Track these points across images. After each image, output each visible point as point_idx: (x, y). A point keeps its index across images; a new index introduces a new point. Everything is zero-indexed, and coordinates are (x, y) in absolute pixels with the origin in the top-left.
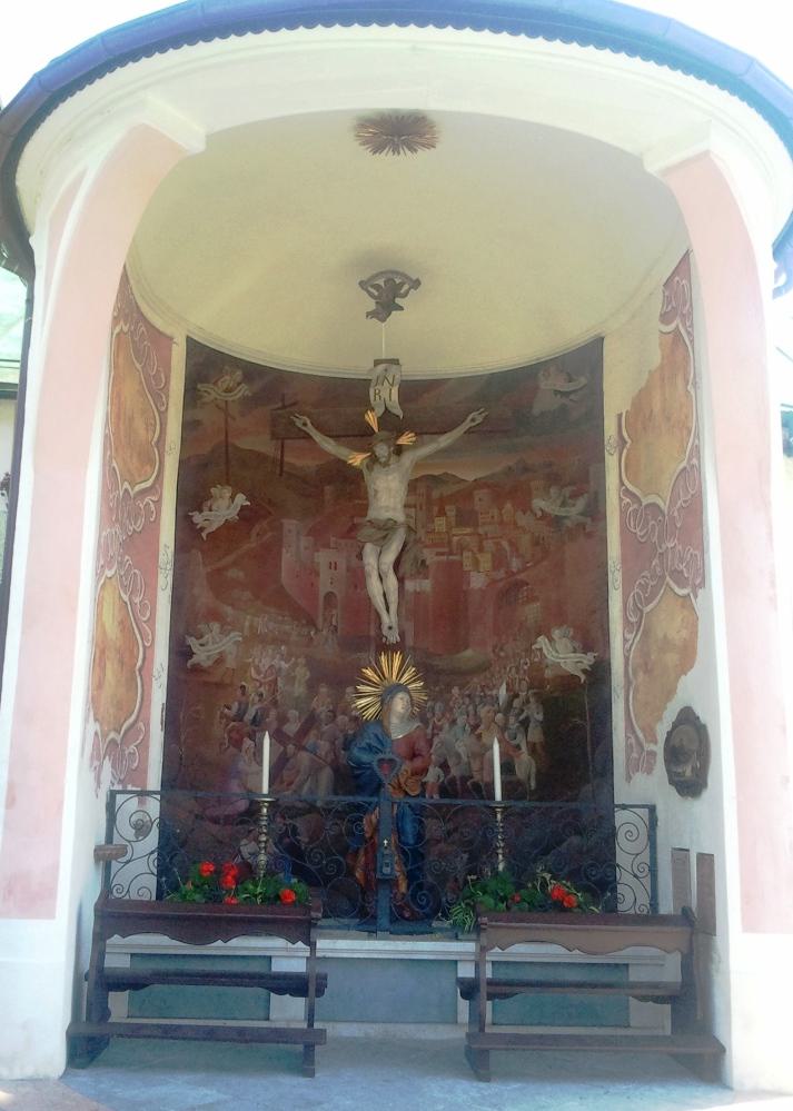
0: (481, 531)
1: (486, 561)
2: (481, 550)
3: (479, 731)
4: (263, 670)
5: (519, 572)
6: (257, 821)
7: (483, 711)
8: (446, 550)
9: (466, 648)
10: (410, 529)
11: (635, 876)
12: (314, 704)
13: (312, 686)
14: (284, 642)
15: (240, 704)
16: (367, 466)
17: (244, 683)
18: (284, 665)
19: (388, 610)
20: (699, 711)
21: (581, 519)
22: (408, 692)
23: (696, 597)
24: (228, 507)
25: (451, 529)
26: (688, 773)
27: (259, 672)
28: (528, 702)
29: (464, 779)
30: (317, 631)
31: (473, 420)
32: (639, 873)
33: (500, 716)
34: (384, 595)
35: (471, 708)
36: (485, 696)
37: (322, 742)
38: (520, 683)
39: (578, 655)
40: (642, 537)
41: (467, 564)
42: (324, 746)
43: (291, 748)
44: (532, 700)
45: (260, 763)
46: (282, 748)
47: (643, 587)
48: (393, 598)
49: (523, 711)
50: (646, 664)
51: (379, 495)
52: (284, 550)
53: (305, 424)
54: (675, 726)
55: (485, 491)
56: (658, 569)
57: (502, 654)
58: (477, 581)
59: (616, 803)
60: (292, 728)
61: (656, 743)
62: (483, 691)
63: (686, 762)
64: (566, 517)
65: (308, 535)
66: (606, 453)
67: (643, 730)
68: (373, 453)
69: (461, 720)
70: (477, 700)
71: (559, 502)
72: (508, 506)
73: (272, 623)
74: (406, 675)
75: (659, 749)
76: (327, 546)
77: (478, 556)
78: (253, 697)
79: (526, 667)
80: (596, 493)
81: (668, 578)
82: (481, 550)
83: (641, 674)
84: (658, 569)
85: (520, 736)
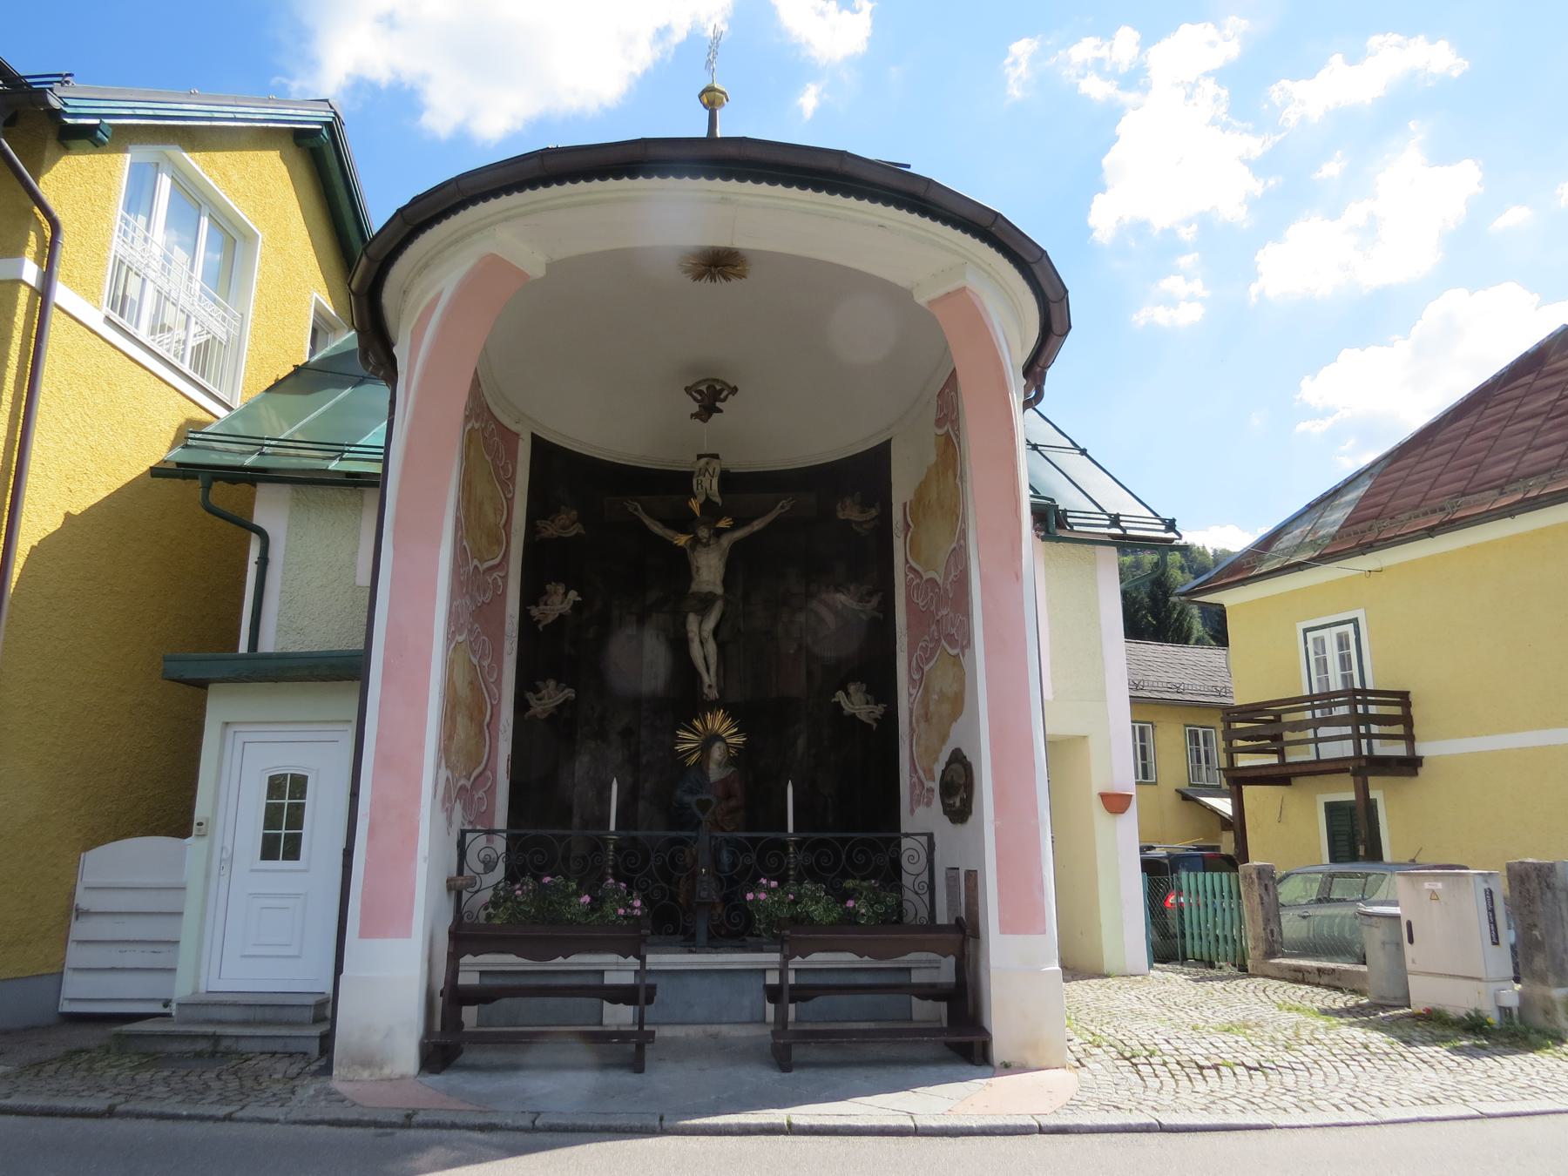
10: (727, 603)
11: (917, 893)
20: (966, 753)
22: (723, 740)
26: (958, 804)
31: (782, 507)
32: (920, 892)
40: (923, 607)
47: (924, 649)
48: (713, 660)
51: (701, 572)
53: (636, 509)
54: (948, 764)
56: (936, 634)
61: (934, 781)
63: (956, 794)
67: (924, 772)
75: (936, 785)
84: (936, 634)
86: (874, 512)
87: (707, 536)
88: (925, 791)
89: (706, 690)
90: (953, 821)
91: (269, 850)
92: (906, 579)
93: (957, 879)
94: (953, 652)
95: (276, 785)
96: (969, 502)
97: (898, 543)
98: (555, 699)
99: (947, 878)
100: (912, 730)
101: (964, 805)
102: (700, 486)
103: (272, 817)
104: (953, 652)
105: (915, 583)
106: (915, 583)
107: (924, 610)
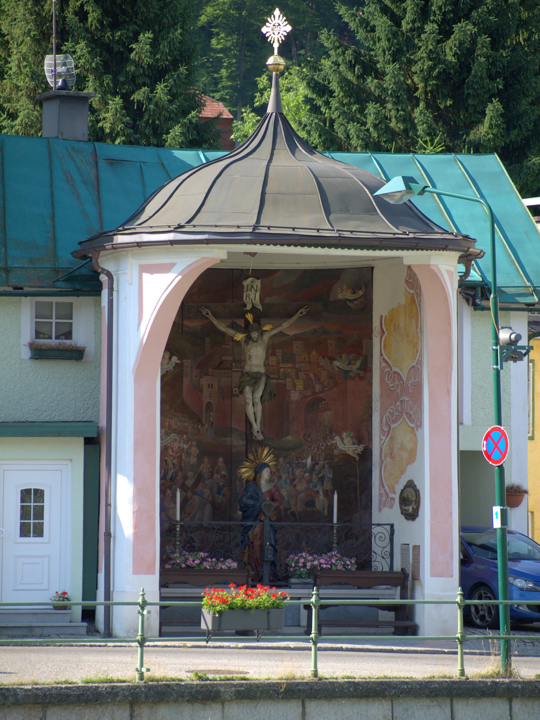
0: (297, 366)
1: (300, 386)
2: (297, 377)
3: (294, 483)
4: (175, 450)
5: (320, 392)
6: (174, 536)
7: (298, 472)
8: (276, 376)
9: (287, 435)
10: (268, 377)
11: (383, 558)
12: (201, 468)
13: (200, 458)
14: (186, 433)
15: (165, 470)
16: (245, 342)
17: (166, 458)
18: (186, 446)
19: (256, 421)
20: (416, 483)
21: (358, 371)
22: (269, 466)
23: (417, 431)
24: (168, 364)
25: (279, 363)
26: (410, 510)
27: (173, 451)
28: (324, 467)
29: (286, 510)
30: (202, 425)
31: (301, 313)
32: (385, 557)
33: (307, 474)
34: (254, 414)
35: (290, 469)
36: (299, 463)
37: (206, 490)
38: (319, 457)
39: (356, 446)
40: (392, 387)
41: (289, 386)
42: (207, 492)
43: (189, 494)
44: (326, 466)
45: (175, 502)
46: (185, 494)
47: (392, 414)
48: (259, 415)
49: (320, 472)
50: (392, 454)
51: (252, 358)
52: (184, 379)
53: (207, 314)
54: (405, 487)
55: (301, 342)
56: (400, 408)
57: (309, 439)
58: (295, 396)
59: (373, 523)
60: (189, 483)
61: (395, 494)
62: (297, 460)
63: (410, 505)
64: (351, 371)
65: (197, 368)
66: (374, 336)
67: (389, 487)
68: (249, 335)
69: (284, 476)
70: (294, 465)
71: (347, 363)
72: (314, 352)
73: (179, 423)
74: (269, 458)
75: (397, 497)
76: (207, 374)
77: (295, 381)
78: (171, 465)
79: (323, 448)
80: (366, 357)
81: (404, 415)
82: (297, 377)
83: (388, 459)
84: (400, 408)
85: (318, 486)
86: (361, 293)
87: (257, 337)
88: (389, 499)
89: (255, 434)
90: (407, 518)
91: (24, 531)
92: (380, 366)
93: (408, 550)
94: (412, 425)
95: (26, 494)
96: (425, 349)
97: (376, 340)
98: (166, 440)
99: (402, 550)
100: (382, 462)
101: (414, 512)
102: (248, 298)
103: (25, 513)
104: (412, 425)
105: (386, 370)
106: (386, 370)
107: (392, 389)
